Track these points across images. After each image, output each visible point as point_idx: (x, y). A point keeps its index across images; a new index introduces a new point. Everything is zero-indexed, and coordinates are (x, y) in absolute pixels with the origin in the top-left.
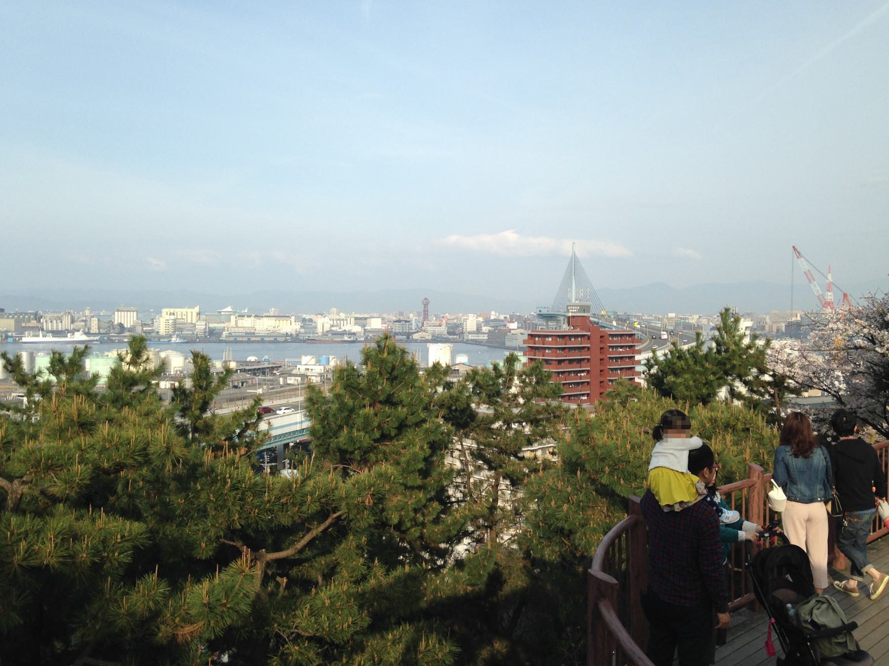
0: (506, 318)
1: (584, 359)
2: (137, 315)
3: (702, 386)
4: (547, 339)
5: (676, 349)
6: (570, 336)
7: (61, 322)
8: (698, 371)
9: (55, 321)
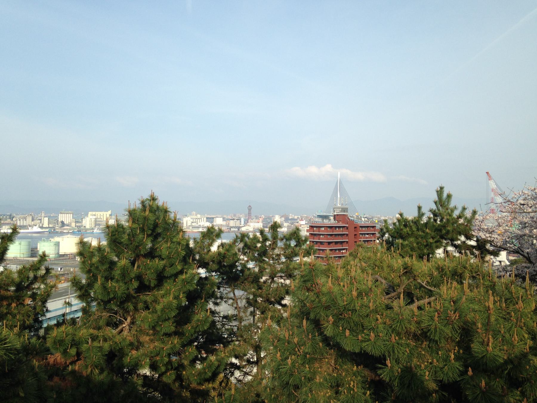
0: (298, 218)
1: (344, 242)
2: (73, 216)
3: (423, 248)
4: (321, 229)
5: (403, 218)
6: (336, 227)
7: (26, 220)
8: (420, 235)
9: (22, 220)
